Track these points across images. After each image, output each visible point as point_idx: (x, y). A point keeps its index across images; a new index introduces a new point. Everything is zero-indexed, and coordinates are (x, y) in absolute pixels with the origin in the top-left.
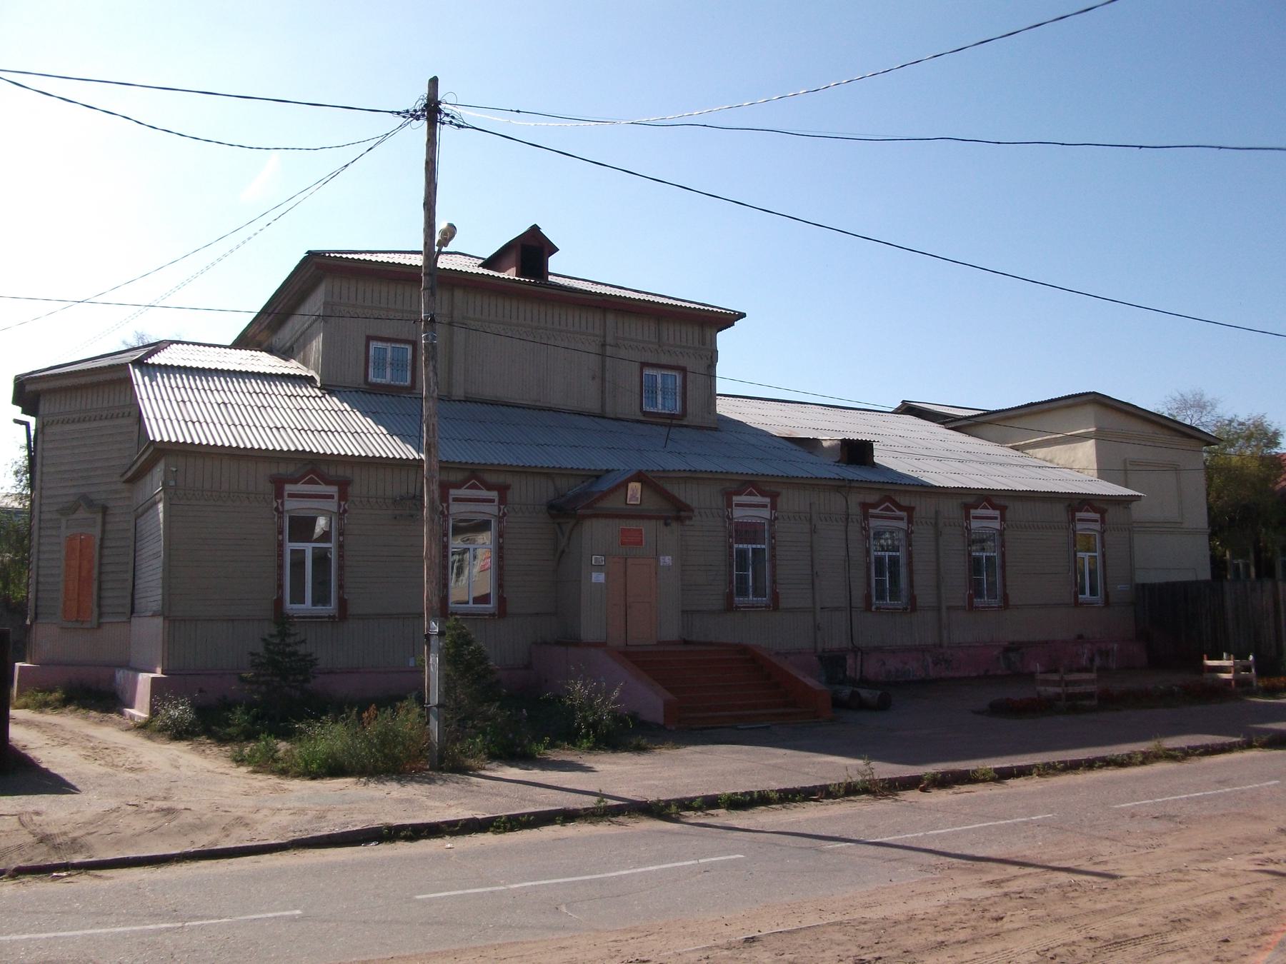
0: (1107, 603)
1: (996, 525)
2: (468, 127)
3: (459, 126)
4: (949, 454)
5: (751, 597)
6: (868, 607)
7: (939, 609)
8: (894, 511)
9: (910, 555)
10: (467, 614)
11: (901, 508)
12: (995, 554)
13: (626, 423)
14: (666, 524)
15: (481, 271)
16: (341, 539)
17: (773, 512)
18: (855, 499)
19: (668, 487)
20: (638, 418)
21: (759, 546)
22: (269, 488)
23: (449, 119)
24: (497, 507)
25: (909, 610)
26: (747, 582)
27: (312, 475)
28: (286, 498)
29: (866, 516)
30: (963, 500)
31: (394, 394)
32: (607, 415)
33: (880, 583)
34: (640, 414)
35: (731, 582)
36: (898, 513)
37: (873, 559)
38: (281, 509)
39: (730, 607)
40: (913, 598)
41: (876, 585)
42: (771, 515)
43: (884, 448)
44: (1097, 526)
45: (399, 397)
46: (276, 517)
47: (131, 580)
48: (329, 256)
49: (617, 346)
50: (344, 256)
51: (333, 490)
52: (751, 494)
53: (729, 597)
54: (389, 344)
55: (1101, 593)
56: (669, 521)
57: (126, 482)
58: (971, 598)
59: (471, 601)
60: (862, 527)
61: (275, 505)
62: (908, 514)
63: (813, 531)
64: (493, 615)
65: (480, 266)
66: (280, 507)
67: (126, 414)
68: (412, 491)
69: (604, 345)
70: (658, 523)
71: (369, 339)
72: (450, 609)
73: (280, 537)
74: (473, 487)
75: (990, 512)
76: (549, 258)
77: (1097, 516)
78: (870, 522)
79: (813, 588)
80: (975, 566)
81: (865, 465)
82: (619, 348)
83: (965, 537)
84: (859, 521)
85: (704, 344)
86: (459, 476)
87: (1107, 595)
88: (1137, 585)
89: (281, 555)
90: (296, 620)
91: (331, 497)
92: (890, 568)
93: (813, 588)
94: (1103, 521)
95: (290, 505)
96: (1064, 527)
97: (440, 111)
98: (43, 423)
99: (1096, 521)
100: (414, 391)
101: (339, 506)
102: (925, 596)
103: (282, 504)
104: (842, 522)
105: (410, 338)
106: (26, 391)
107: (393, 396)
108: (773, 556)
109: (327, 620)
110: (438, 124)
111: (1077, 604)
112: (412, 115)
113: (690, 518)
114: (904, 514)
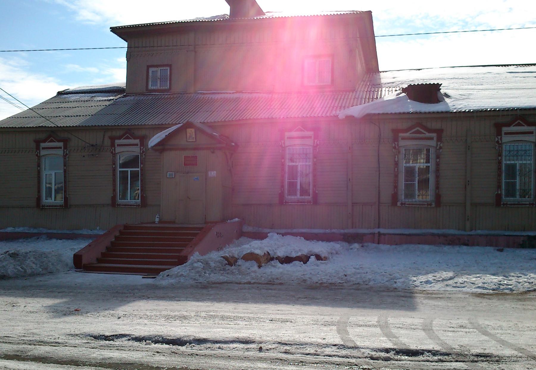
11: (430, 131)
22: (33, 145)
24: (139, 148)
27: (519, 121)
28: (503, 135)
36: (428, 135)
38: (500, 142)
42: (314, 143)
46: (497, 147)
51: (61, 144)
53: (499, 197)
61: (497, 139)
66: (499, 140)
73: (500, 158)
86: (118, 133)
89: (500, 169)
90: (45, 207)
93: (465, 190)
103: (501, 139)
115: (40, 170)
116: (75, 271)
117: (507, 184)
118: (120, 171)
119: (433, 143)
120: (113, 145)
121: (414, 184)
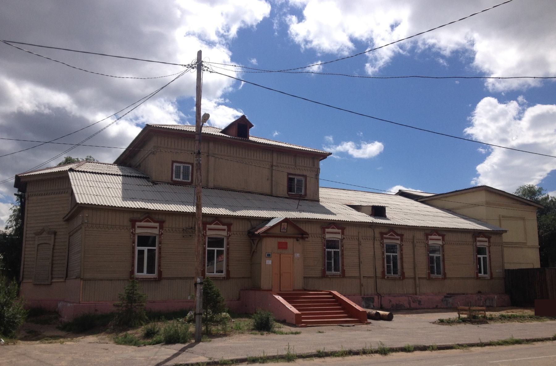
0: (492, 278)
1: (440, 243)
2: (214, 72)
3: (211, 72)
4: (419, 212)
5: (333, 271)
6: (383, 277)
7: (414, 278)
8: (394, 236)
9: (402, 255)
10: (213, 278)
11: (398, 235)
12: (440, 255)
13: (281, 199)
14: (297, 240)
15: (221, 134)
16: (160, 245)
17: (343, 236)
18: (377, 231)
19: (298, 225)
20: (287, 196)
21: (336, 250)
23: (206, 69)
24: (227, 233)
25: (401, 279)
26: (331, 265)
29: (382, 238)
30: (426, 232)
31: (184, 185)
32: (273, 195)
33: (389, 267)
34: (287, 194)
35: (325, 265)
36: (396, 237)
37: (385, 256)
38: (134, 233)
39: (324, 276)
40: (403, 274)
41: (387, 268)
43: (391, 210)
44: (486, 244)
45: (186, 186)
47: (66, 263)
48: (156, 127)
49: (277, 166)
50: (162, 127)
51: (157, 225)
52: (333, 228)
53: (324, 272)
54: (182, 165)
55: (489, 273)
56: (299, 239)
57: (65, 221)
58: (429, 274)
59: (215, 272)
60: (381, 243)
61: (131, 231)
62: (401, 238)
63: (360, 244)
64: (224, 278)
65: (220, 132)
67: (66, 192)
68: (191, 225)
69: (272, 166)
70: (255, 153)
71: (173, 162)
72: (206, 275)
73: (133, 245)
74: (217, 224)
75: (437, 237)
76: (250, 130)
77: (487, 239)
78: (384, 240)
79: (360, 268)
80: (431, 260)
81: (382, 216)
82: (279, 167)
83: (426, 248)
84: (379, 240)
85: (314, 166)
87: (491, 273)
88: (505, 270)
91: (156, 228)
92: (393, 260)
93: (360, 268)
94: (489, 242)
95: (138, 231)
96: (471, 244)
97: (202, 65)
98: (28, 195)
99: (486, 242)
100: (192, 184)
101: (160, 231)
102: (408, 273)
103: (135, 231)
104: (372, 240)
105: (191, 162)
106: (21, 181)
107: (183, 186)
108: (342, 254)
109: (153, 280)
110: (202, 71)
111: (478, 278)
112: (191, 67)
113: (307, 238)
114: (399, 237)
115: (161, 246)
116: (442, 322)
117: (387, 266)
118: (208, 250)
119: (399, 242)
120: (204, 229)
121: (391, 266)
